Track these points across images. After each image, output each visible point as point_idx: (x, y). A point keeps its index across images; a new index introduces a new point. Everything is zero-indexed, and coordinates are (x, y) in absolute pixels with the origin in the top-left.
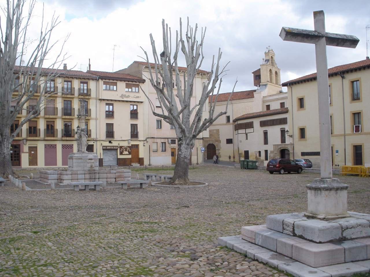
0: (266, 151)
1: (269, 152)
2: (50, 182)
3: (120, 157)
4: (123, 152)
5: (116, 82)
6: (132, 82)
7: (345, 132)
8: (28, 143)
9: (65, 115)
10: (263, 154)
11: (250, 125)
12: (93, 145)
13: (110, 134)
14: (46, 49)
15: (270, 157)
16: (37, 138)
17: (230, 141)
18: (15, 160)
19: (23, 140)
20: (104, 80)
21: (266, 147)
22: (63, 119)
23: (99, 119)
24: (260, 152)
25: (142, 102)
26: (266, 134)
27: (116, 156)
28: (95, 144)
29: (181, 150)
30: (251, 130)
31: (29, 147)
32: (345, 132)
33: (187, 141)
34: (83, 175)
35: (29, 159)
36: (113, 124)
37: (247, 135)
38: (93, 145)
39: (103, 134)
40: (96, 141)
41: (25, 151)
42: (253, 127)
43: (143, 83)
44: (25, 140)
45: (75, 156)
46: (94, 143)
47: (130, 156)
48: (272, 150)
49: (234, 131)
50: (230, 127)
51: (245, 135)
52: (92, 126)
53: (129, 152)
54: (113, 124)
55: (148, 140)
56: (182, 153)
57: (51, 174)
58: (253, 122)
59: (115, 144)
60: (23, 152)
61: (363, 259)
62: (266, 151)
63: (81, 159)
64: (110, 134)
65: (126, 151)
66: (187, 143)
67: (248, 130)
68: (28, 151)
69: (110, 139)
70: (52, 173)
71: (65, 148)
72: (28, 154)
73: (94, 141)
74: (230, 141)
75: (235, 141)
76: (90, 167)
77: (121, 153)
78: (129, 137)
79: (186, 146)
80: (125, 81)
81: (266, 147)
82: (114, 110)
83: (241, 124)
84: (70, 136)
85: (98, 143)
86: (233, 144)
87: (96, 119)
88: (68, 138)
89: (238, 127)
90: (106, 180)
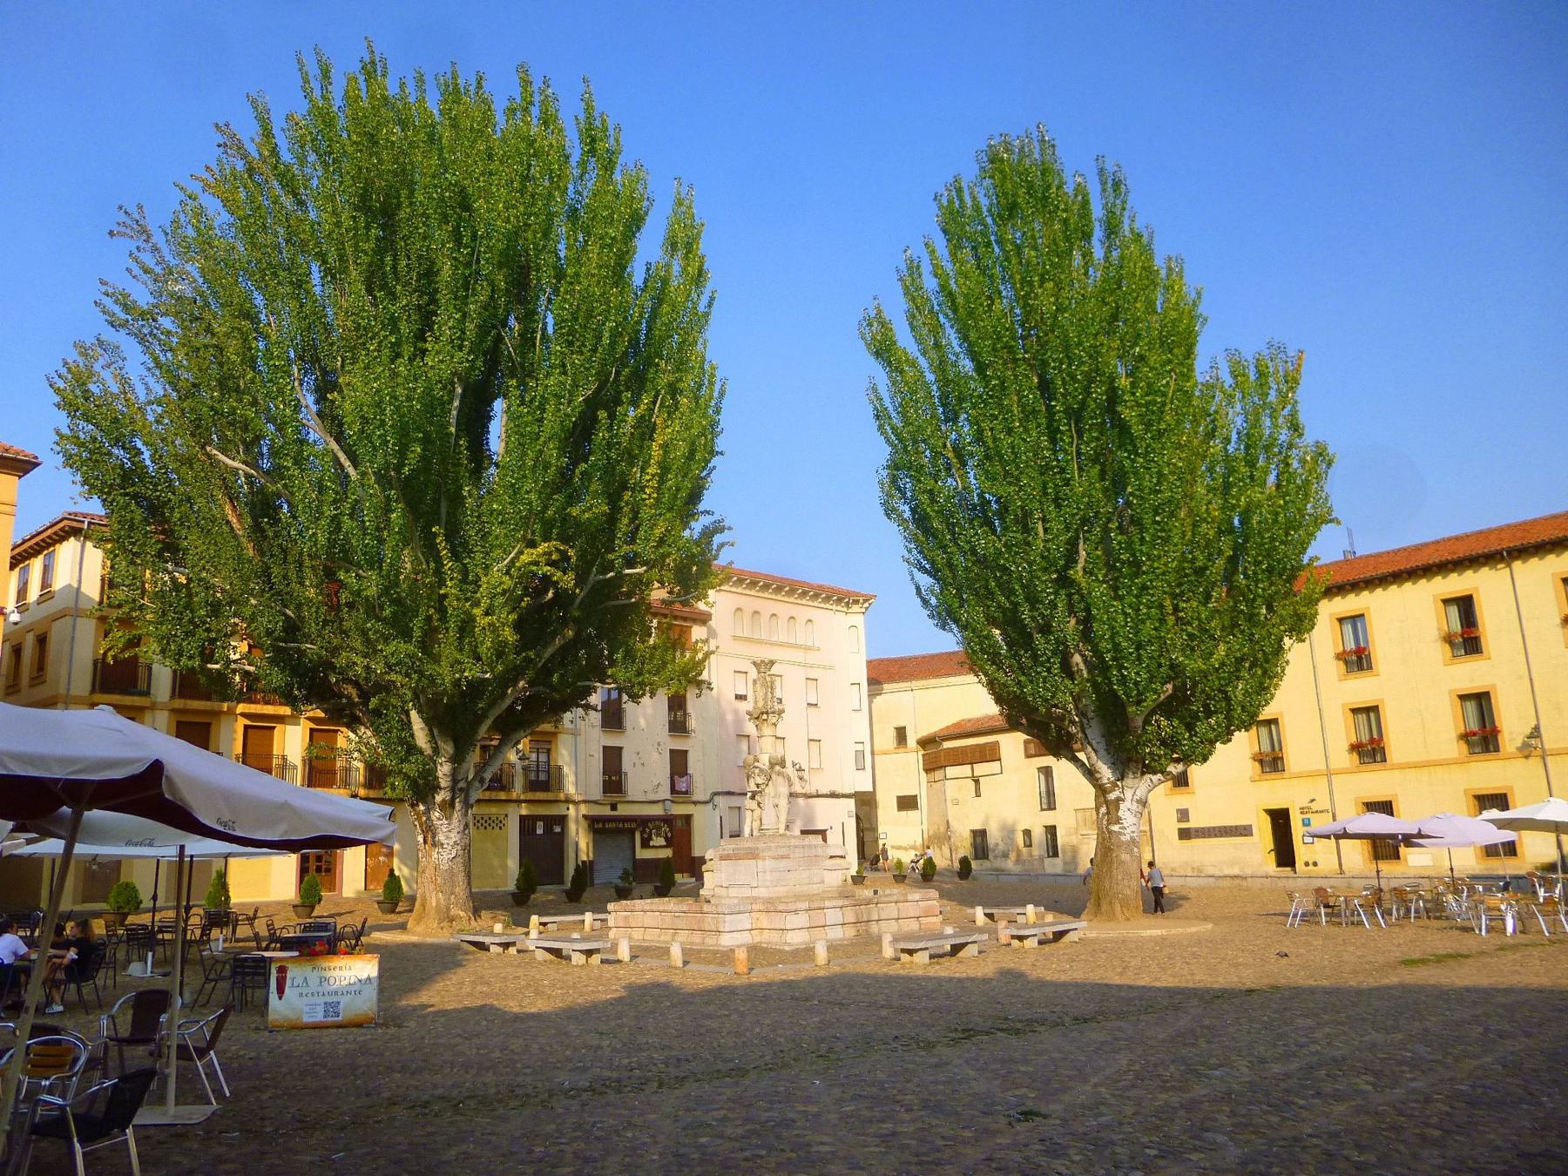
3: (642, 854)
4: (650, 838)
7: (1330, 785)
9: (182, 696)
11: (990, 754)
13: (614, 780)
16: (503, 796)
17: (907, 803)
21: (1049, 818)
22: (174, 711)
27: (628, 853)
30: (993, 767)
32: (1330, 785)
36: (620, 749)
37: (977, 782)
47: (667, 853)
49: (923, 774)
50: (913, 759)
53: (666, 839)
54: (620, 749)
55: (717, 799)
59: (623, 810)
61: (1423, 757)
62: (1051, 830)
64: (614, 780)
65: (658, 835)
67: (980, 769)
69: (615, 798)
74: (907, 803)
77: (645, 844)
78: (665, 792)
79: (1135, 806)
81: (1049, 818)
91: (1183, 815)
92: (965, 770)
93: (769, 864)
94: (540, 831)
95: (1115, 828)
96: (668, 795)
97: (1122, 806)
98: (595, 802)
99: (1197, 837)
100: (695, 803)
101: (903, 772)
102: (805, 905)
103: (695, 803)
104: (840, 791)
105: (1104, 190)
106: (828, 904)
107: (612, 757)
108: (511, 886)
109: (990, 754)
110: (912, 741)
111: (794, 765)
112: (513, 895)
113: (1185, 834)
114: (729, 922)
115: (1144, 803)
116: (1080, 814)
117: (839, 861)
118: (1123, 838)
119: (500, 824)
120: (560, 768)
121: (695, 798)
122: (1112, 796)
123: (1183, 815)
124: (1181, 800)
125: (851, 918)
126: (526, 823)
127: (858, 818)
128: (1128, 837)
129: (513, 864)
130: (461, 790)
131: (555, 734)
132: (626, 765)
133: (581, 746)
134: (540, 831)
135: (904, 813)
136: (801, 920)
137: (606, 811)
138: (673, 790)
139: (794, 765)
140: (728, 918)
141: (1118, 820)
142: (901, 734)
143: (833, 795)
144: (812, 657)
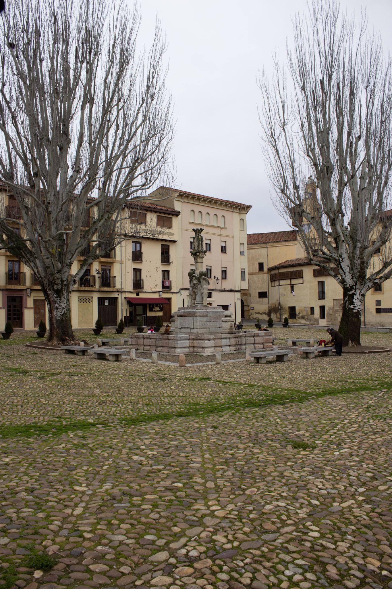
0: (322, 308)
1: (326, 309)
2: (178, 350)
5: (146, 212)
6: (164, 213)
8: (33, 294)
10: (317, 311)
11: (299, 275)
12: (117, 298)
13: (138, 284)
14: (360, 117)
15: (327, 314)
17: (263, 295)
18: (15, 319)
19: (26, 290)
20: (131, 210)
21: (322, 303)
23: (124, 262)
24: (312, 309)
25: (175, 242)
26: (322, 284)
28: (119, 297)
29: (354, 303)
30: (300, 281)
31: (34, 300)
33: (362, 291)
34: (228, 340)
35: (34, 317)
38: (117, 298)
39: (128, 286)
40: (121, 292)
41: (28, 306)
42: (302, 278)
43: (177, 216)
44: (29, 291)
45: (199, 312)
46: (285, 289)
48: (331, 305)
49: (270, 282)
50: (265, 277)
51: (289, 288)
52: (116, 271)
53: (160, 308)
55: (182, 291)
56: (355, 307)
57: (181, 340)
58: (302, 270)
59: (142, 296)
60: (27, 308)
62: (322, 308)
63: (207, 316)
64: (138, 284)
66: (361, 294)
67: (294, 282)
68: (32, 306)
69: (138, 290)
70: (183, 338)
71: (82, 303)
72: (33, 310)
73: (117, 293)
74: (263, 295)
75: (270, 294)
76: (229, 327)
78: (159, 288)
80: (156, 212)
81: (322, 303)
82: (142, 251)
83: (284, 273)
84: (109, 285)
85: (124, 295)
86: (267, 299)
87: (121, 263)
88: (87, 289)
89: (274, 278)
90: (253, 346)
91: (378, 303)
92: (288, 282)
93: (199, 319)
94: (106, 304)
95: (351, 307)
96: (161, 289)
97: (355, 297)
98: (130, 292)
99: (384, 312)
100: (173, 293)
101: (262, 282)
102: (213, 337)
103: (173, 293)
104: (234, 288)
105: (97, 47)
106: (223, 336)
107: (137, 272)
108: (94, 327)
109: (299, 275)
110: (265, 269)
111: (215, 277)
112: (94, 330)
113: (378, 311)
114: (180, 343)
115: (363, 296)
116: (335, 301)
117: (228, 318)
118: (354, 311)
119: (90, 300)
120: (115, 278)
121: (173, 291)
122: (351, 293)
123: (378, 303)
124: (378, 297)
125: (233, 341)
126: (101, 301)
127: (242, 301)
128: (357, 311)
129: (95, 317)
130: (65, 285)
131: (112, 263)
132: (143, 277)
133: (123, 269)
134: (106, 304)
135: (261, 299)
136: (211, 343)
137: (134, 296)
138: (164, 287)
139: (215, 277)
140: (179, 342)
141: (352, 303)
142: (261, 266)
143: (231, 291)
144: (223, 232)
